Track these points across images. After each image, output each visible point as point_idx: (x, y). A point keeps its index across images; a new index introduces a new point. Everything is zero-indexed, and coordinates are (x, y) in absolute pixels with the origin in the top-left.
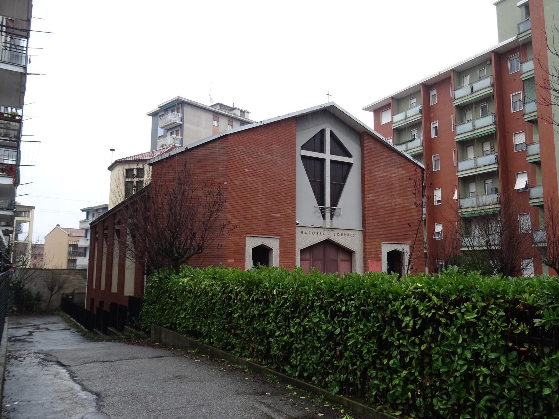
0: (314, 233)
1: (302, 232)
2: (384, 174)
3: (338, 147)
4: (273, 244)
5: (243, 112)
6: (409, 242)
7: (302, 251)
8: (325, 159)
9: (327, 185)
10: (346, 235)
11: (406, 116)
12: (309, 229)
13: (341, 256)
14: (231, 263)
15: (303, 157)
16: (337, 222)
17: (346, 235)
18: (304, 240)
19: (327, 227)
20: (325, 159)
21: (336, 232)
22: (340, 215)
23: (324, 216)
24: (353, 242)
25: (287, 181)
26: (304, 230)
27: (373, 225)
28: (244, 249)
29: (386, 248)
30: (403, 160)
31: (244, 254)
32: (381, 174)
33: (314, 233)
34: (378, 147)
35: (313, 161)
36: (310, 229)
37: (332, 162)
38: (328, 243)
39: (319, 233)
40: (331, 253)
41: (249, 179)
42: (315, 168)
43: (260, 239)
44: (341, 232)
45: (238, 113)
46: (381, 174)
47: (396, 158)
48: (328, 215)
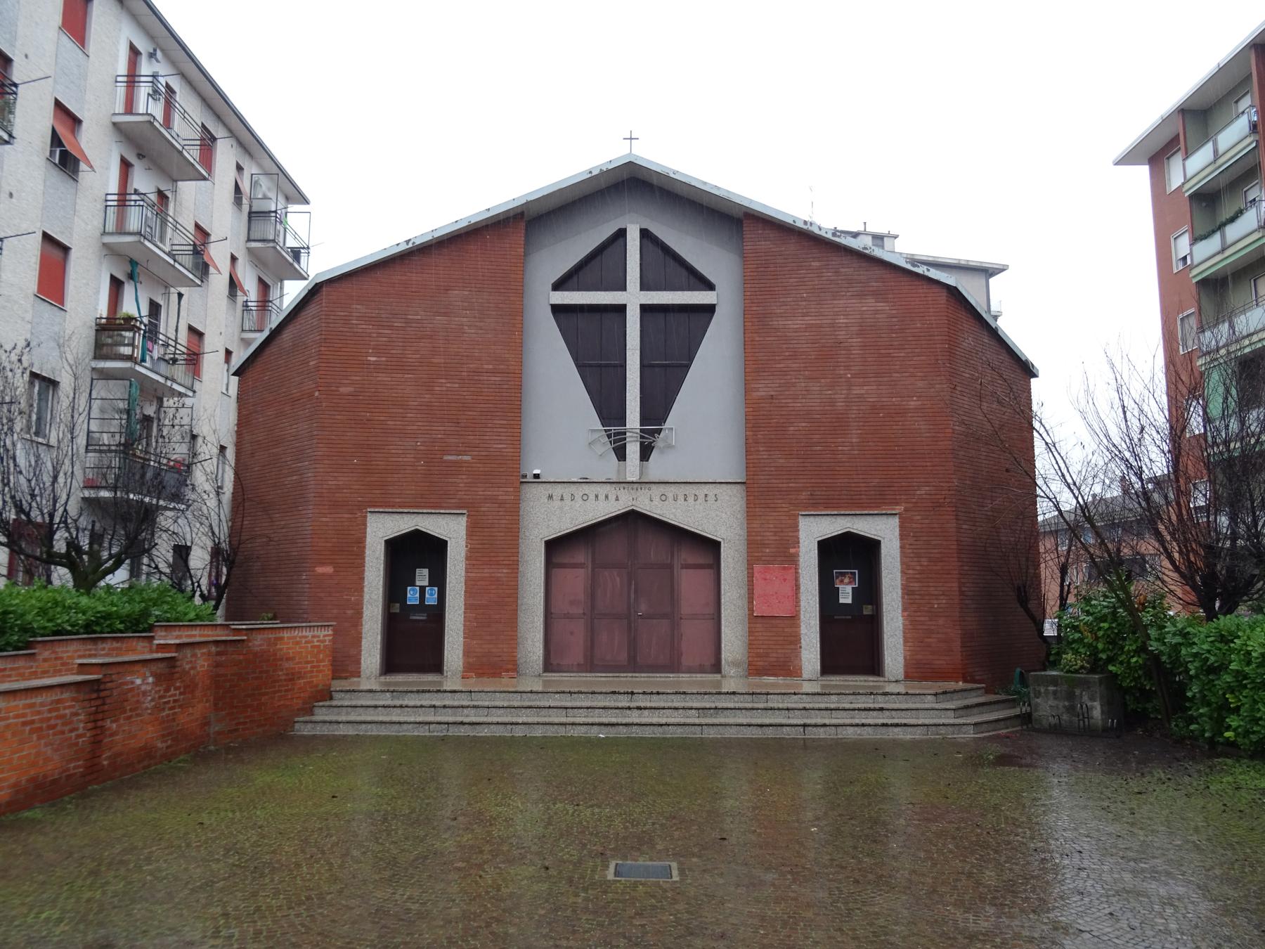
0: (585, 497)
1: (550, 497)
2: (810, 320)
3: (665, 265)
4: (451, 529)
5: (878, 238)
6: (899, 509)
7: (554, 546)
8: (624, 307)
9: (635, 374)
10: (691, 499)
11: (1216, 151)
12: (573, 488)
13: (686, 555)
14: (323, 574)
15: (557, 310)
16: (659, 466)
17: (691, 499)
18: (549, 516)
19: (629, 479)
20: (624, 307)
21: (656, 491)
22: (670, 447)
23: (621, 454)
24: (718, 516)
25: (494, 372)
26: (557, 491)
27: (779, 468)
28: (361, 542)
29: (814, 530)
30: (879, 272)
31: (361, 555)
32: (798, 323)
33: (585, 497)
34: (792, 247)
35: (661, 316)
36: (573, 487)
37: (645, 309)
38: (632, 519)
39: (602, 497)
40: (654, 550)
41: (383, 377)
42: (591, 335)
43: (406, 518)
44: (670, 491)
45: (867, 241)
46: (798, 323)
47: (849, 268)
48: (633, 449)
